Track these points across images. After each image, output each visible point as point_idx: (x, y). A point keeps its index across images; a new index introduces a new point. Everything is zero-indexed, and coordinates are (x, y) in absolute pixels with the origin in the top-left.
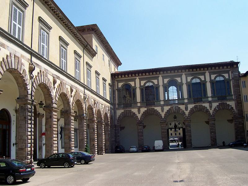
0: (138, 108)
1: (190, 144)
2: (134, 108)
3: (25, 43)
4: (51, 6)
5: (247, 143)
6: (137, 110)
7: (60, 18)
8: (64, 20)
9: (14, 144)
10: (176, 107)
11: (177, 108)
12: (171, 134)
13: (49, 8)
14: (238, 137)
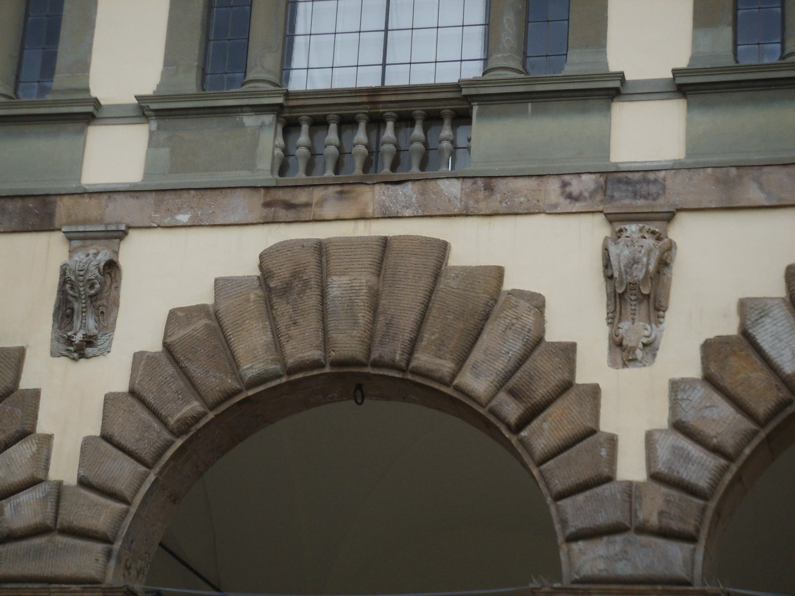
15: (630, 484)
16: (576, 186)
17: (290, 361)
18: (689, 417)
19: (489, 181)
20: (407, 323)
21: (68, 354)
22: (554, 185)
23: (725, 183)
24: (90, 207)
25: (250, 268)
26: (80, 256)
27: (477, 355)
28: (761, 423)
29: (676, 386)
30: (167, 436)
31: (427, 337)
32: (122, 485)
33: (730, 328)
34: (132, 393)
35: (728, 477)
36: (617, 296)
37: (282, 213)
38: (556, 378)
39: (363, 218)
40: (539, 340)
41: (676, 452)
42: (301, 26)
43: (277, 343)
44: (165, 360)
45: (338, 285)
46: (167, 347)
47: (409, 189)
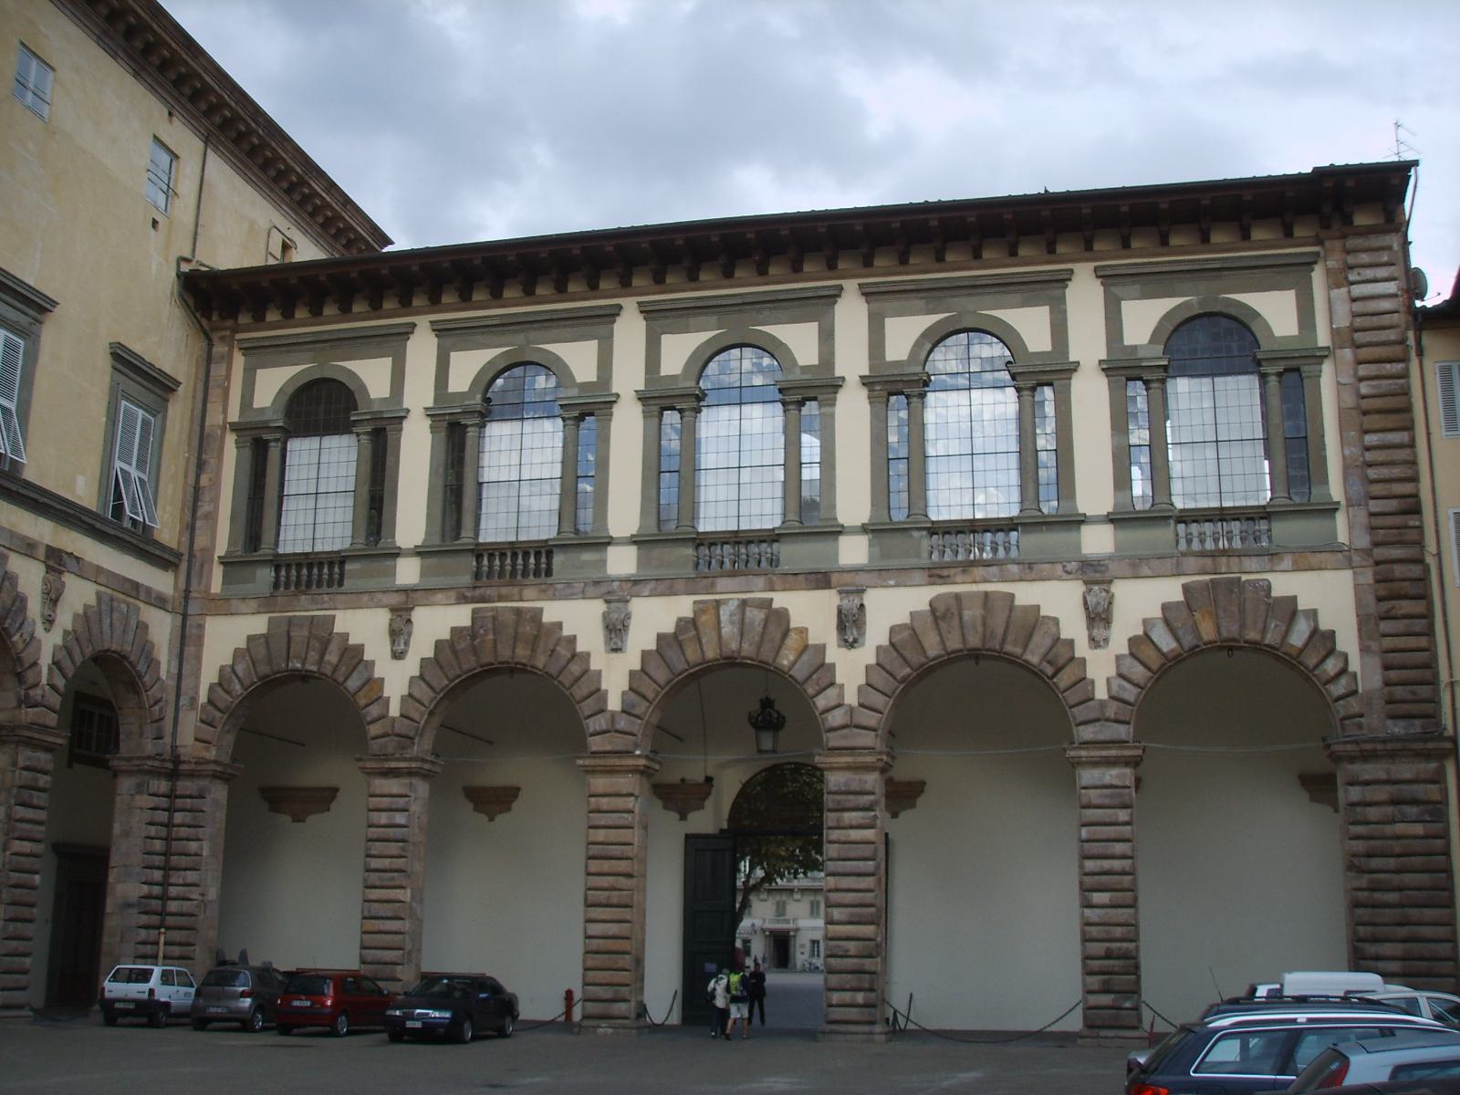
15: (1101, 700)
16: (1069, 567)
17: (949, 650)
18: (1125, 671)
19: (1030, 566)
20: (1000, 630)
21: (846, 647)
22: (1059, 567)
23: (1134, 566)
24: (848, 578)
25: (925, 606)
26: (845, 602)
27: (1031, 646)
28: (1154, 673)
29: (1118, 658)
30: (897, 684)
31: (1010, 638)
32: (879, 707)
33: (1140, 632)
34: (878, 664)
35: (1141, 697)
37: (938, 580)
38: (1068, 656)
39: (975, 582)
40: (1058, 638)
41: (1120, 687)
42: (284, 508)
43: (943, 642)
44: (892, 649)
45: (967, 614)
46: (892, 644)
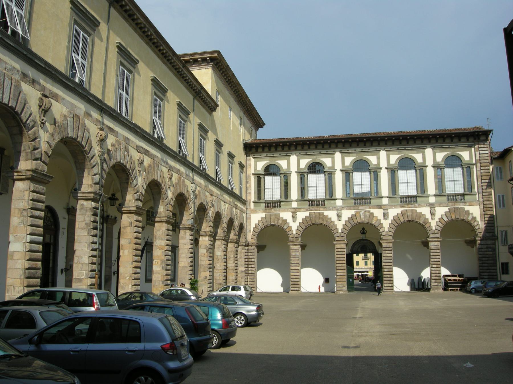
0: (293, 210)
1: (390, 285)
2: (285, 210)
3: (93, 91)
4: (139, 21)
5: (494, 241)
6: (290, 214)
7: (154, 43)
8: (161, 45)
9: (62, 271)
10: (365, 211)
11: (368, 214)
12: (358, 263)
13: (135, 26)
14: (483, 274)
36: (43, 300)
43: (375, 223)
45: (408, 214)
47: (413, 205)
